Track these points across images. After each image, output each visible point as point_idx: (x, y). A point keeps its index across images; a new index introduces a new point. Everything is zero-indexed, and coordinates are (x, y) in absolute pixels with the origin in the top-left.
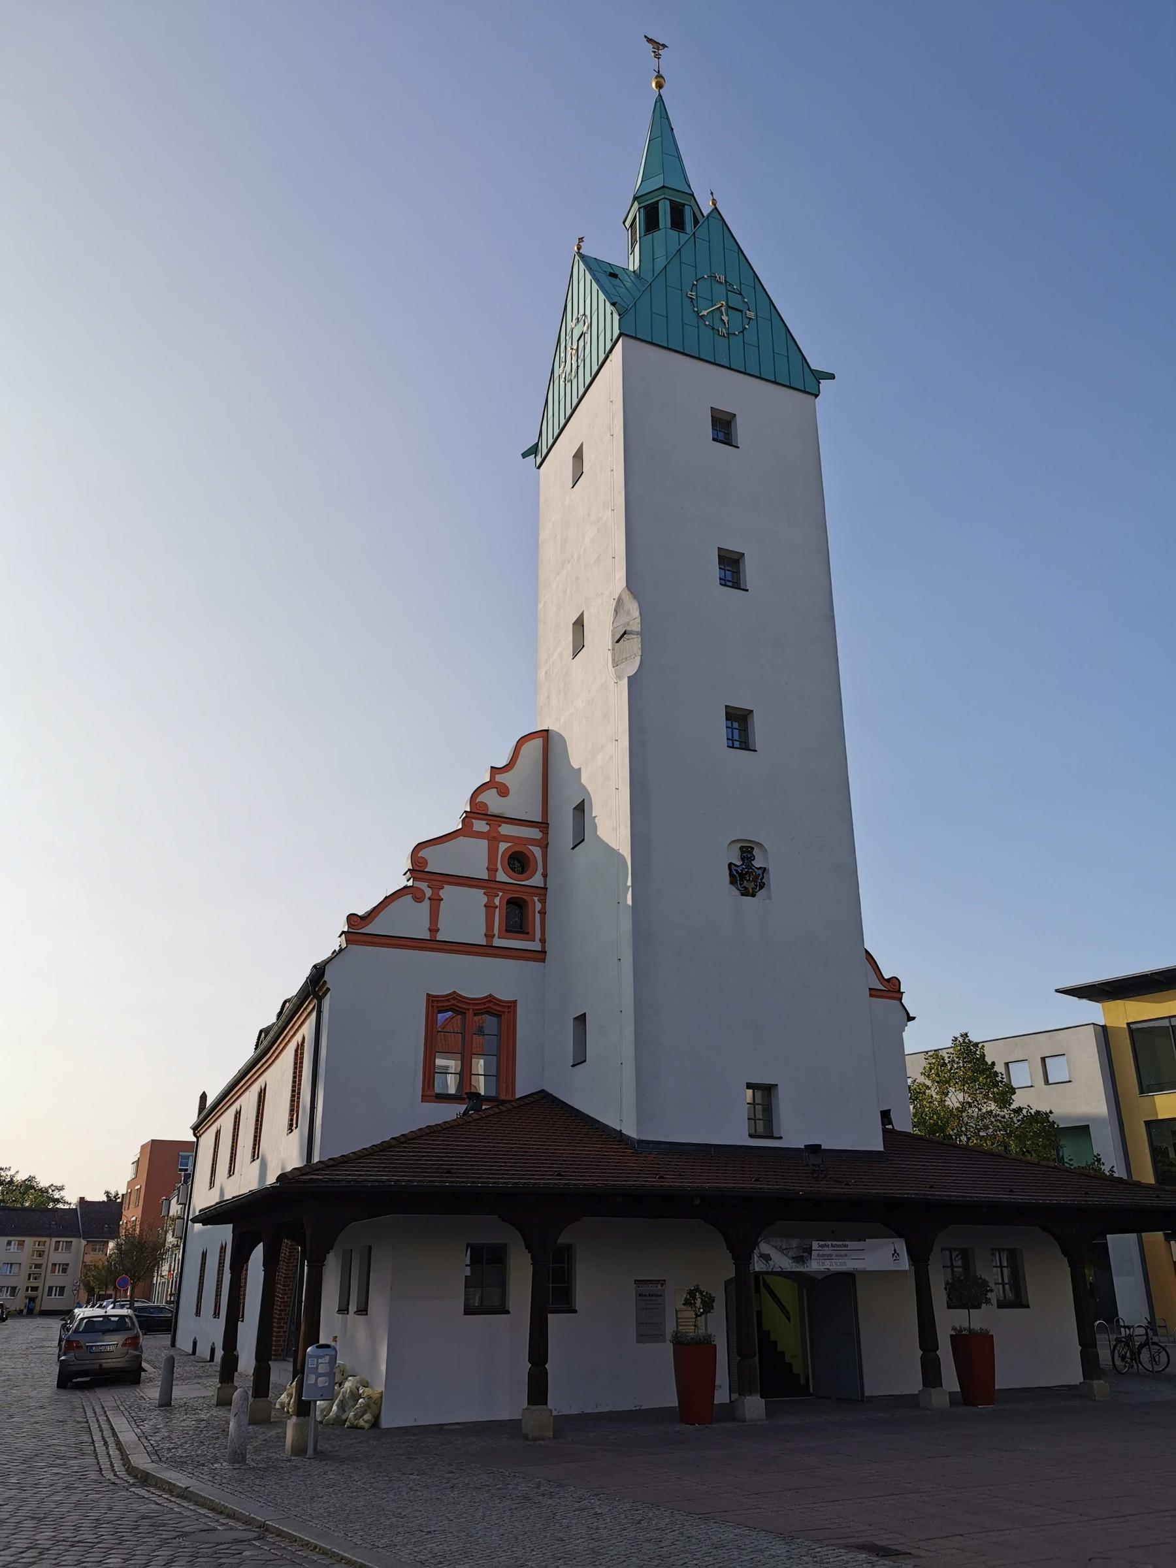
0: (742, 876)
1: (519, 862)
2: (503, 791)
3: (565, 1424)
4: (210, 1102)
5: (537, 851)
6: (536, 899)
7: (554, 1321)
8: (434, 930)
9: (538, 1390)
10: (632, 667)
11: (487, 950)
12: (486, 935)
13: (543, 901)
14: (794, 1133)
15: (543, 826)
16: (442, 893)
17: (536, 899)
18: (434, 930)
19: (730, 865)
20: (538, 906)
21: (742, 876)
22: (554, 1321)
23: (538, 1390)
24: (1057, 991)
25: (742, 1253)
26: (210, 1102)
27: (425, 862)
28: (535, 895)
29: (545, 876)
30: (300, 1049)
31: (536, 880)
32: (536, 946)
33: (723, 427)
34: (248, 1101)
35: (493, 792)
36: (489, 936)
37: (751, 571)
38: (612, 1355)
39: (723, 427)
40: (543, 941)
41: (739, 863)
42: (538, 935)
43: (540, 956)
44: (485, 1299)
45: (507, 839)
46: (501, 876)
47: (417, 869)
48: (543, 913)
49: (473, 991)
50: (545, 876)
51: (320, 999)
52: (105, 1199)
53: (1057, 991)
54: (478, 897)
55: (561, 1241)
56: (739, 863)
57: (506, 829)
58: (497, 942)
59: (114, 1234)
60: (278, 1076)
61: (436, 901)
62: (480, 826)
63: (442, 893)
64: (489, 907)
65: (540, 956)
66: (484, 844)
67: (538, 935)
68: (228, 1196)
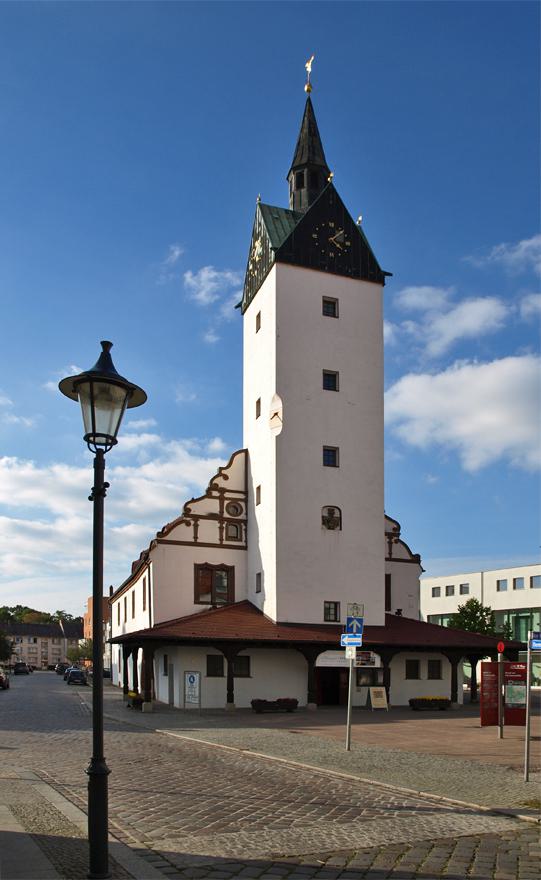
0: (328, 522)
2: (226, 478)
3: (394, 707)
4: (115, 590)
5: (243, 504)
7: (237, 681)
8: (196, 537)
9: (230, 698)
10: (278, 431)
11: (221, 546)
18: (196, 537)
20: (244, 527)
21: (328, 522)
22: (237, 681)
23: (230, 698)
25: (312, 659)
26: (115, 590)
27: (190, 510)
29: (247, 514)
30: (144, 580)
31: (242, 517)
32: (242, 544)
33: (330, 307)
34: (128, 594)
35: (221, 478)
36: (221, 539)
39: (330, 307)
40: (246, 542)
42: (244, 539)
43: (245, 548)
44: (213, 670)
45: (227, 499)
46: (226, 515)
47: (187, 511)
48: (246, 530)
50: (247, 514)
51: (149, 565)
54: (216, 524)
55: (426, 620)
57: (227, 495)
58: (225, 542)
59: (82, 636)
60: (138, 586)
61: (196, 526)
62: (215, 493)
64: (221, 528)
65: (245, 548)
66: (218, 501)
67: (244, 539)
68: (128, 632)
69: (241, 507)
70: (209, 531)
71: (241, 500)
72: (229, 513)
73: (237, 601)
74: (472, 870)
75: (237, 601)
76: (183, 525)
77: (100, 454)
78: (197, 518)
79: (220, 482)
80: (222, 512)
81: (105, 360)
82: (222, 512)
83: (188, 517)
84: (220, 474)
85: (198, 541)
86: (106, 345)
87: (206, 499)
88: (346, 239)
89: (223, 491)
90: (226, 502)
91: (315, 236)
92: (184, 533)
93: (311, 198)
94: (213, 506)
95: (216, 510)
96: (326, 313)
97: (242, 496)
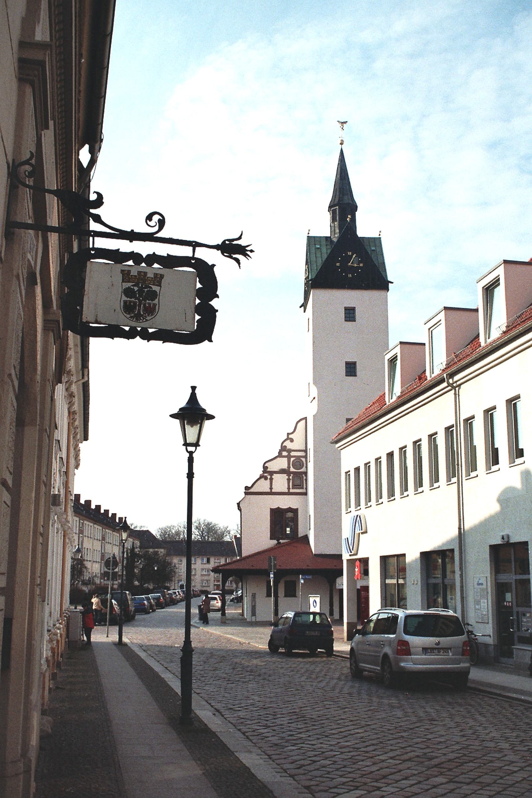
2: (292, 440)
5: (304, 460)
8: (271, 488)
16: (273, 477)
18: (271, 488)
20: (305, 478)
31: (303, 470)
32: (304, 491)
33: (350, 314)
36: (289, 488)
39: (350, 314)
40: (306, 489)
42: (305, 487)
46: (292, 469)
47: (265, 468)
48: (306, 480)
54: (285, 476)
57: (293, 454)
58: (291, 491)
61: (271, 479)
62: (285, 453)
63: (273, 477)
64: (289, 480)
67: (305, 487)
69: (303, 462)
70: (281, 483)
71: (302, 457)
72: (294, 468)
73: (299, 536)
74: (345, 689)
75: (299, 536)
76: (263, 479)
77: (191, 453)
78: (272, 473)
79: (288, 444)
80: (289, 467)
81: (193, 398)
82: (289, 467)
83: (267, 473)
84: (288, 439)
85: (273, 491)
86: (194, 388)
87: (278, 458)
88: (359, 262)
89: (289, 451)
90: (292, 459)
91: (338, 264)
92: (264, 486)
93: (340, 228)
94: (283, 463)
95: (285, 466)
96: (353, 309)
97: (303, 454)
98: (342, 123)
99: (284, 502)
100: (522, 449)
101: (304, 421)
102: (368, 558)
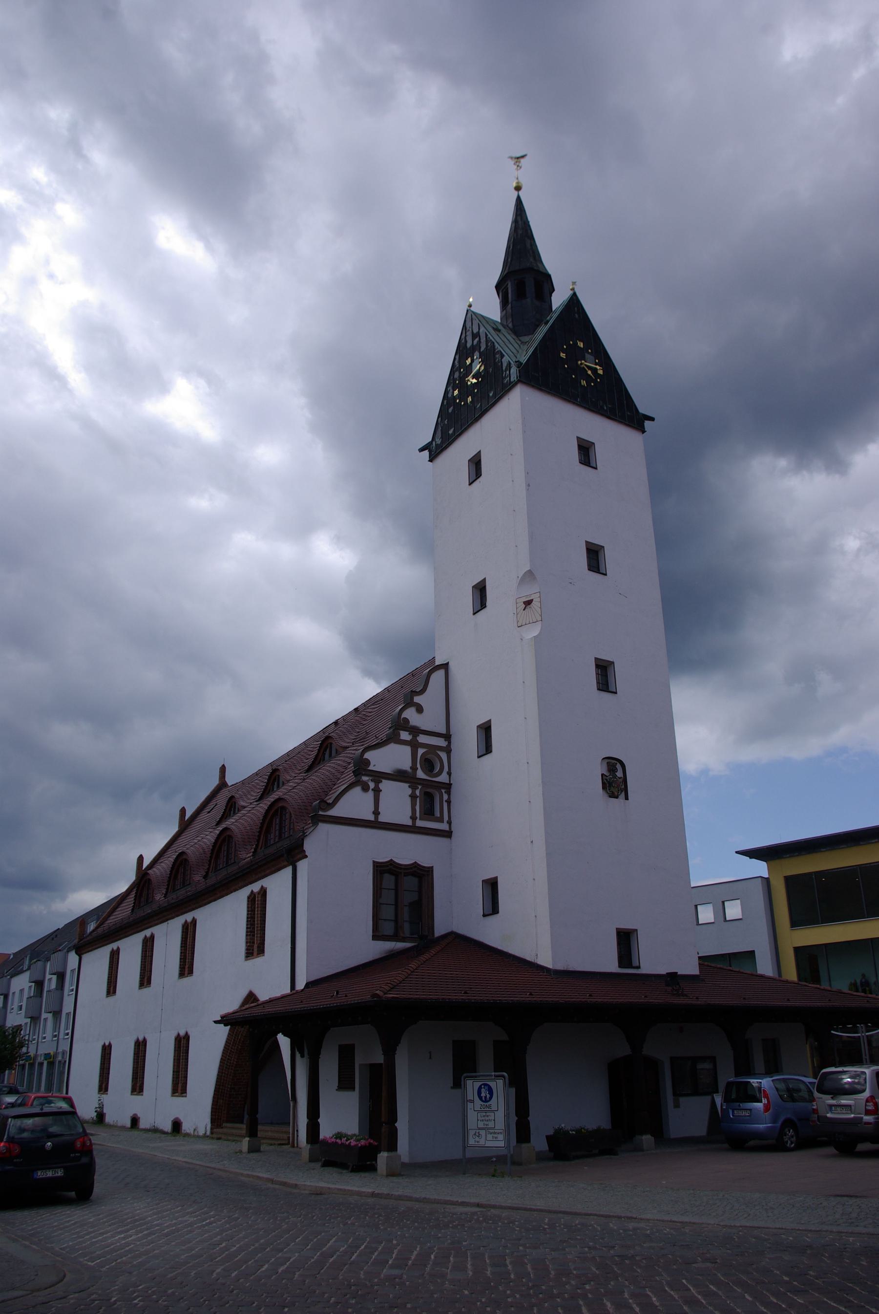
1: (429, 765)
2: (420, 709)
5: (443, 755)
6: (443, 791)
8: (376, 813)
11: (412, 829)
12: (411, 818)
13: (449, 793)
14: (652, 960)
15: (447, 737)
16: (381, 786)
17: (443, 791)
18: (376, 813)
19: (602, 775)
20: (445, 797)
24: (737, 852)
28: (444, 788)
29: (449, 774)
32: (444, 826)
33: (586, 452)
36: (413, 818)
37: (610, 558)
38: (574, 1099)
39: (586, 452)
40: (449, 823)
41: (607, 774)
43: (448, 834)
45: (423, 745)
46: (420, 774)
48: (449, 802)
49: (404, 860)
52: (609, 963)
53: (737, 852)
56: (607, 774)
57: (422, 739)
58: (420, 823)
61: (377, 791)
63: (381, 786)
64: (413, 797)
78: (379, 777)
82: (414, 768)
85: (381, 819)
89: (416, 731)
90: (421, 751)
98: (518, 158)
99: (407, 850)
100: (704, 960)
101: (442, 672)
102: (496, 878)
